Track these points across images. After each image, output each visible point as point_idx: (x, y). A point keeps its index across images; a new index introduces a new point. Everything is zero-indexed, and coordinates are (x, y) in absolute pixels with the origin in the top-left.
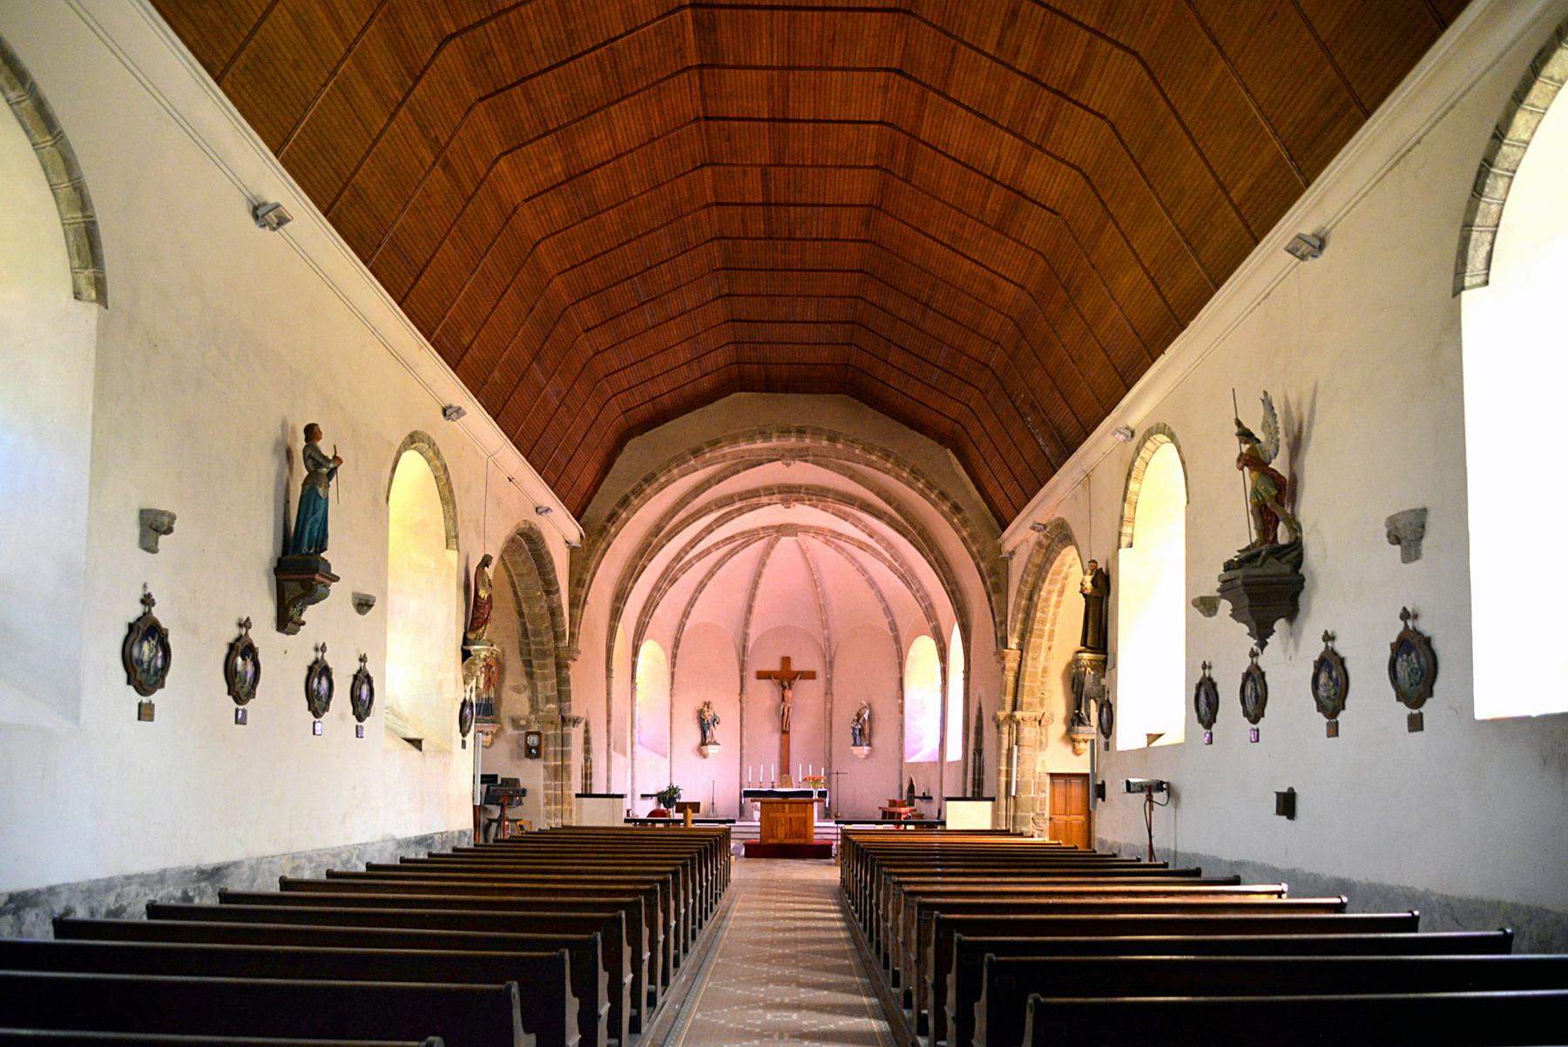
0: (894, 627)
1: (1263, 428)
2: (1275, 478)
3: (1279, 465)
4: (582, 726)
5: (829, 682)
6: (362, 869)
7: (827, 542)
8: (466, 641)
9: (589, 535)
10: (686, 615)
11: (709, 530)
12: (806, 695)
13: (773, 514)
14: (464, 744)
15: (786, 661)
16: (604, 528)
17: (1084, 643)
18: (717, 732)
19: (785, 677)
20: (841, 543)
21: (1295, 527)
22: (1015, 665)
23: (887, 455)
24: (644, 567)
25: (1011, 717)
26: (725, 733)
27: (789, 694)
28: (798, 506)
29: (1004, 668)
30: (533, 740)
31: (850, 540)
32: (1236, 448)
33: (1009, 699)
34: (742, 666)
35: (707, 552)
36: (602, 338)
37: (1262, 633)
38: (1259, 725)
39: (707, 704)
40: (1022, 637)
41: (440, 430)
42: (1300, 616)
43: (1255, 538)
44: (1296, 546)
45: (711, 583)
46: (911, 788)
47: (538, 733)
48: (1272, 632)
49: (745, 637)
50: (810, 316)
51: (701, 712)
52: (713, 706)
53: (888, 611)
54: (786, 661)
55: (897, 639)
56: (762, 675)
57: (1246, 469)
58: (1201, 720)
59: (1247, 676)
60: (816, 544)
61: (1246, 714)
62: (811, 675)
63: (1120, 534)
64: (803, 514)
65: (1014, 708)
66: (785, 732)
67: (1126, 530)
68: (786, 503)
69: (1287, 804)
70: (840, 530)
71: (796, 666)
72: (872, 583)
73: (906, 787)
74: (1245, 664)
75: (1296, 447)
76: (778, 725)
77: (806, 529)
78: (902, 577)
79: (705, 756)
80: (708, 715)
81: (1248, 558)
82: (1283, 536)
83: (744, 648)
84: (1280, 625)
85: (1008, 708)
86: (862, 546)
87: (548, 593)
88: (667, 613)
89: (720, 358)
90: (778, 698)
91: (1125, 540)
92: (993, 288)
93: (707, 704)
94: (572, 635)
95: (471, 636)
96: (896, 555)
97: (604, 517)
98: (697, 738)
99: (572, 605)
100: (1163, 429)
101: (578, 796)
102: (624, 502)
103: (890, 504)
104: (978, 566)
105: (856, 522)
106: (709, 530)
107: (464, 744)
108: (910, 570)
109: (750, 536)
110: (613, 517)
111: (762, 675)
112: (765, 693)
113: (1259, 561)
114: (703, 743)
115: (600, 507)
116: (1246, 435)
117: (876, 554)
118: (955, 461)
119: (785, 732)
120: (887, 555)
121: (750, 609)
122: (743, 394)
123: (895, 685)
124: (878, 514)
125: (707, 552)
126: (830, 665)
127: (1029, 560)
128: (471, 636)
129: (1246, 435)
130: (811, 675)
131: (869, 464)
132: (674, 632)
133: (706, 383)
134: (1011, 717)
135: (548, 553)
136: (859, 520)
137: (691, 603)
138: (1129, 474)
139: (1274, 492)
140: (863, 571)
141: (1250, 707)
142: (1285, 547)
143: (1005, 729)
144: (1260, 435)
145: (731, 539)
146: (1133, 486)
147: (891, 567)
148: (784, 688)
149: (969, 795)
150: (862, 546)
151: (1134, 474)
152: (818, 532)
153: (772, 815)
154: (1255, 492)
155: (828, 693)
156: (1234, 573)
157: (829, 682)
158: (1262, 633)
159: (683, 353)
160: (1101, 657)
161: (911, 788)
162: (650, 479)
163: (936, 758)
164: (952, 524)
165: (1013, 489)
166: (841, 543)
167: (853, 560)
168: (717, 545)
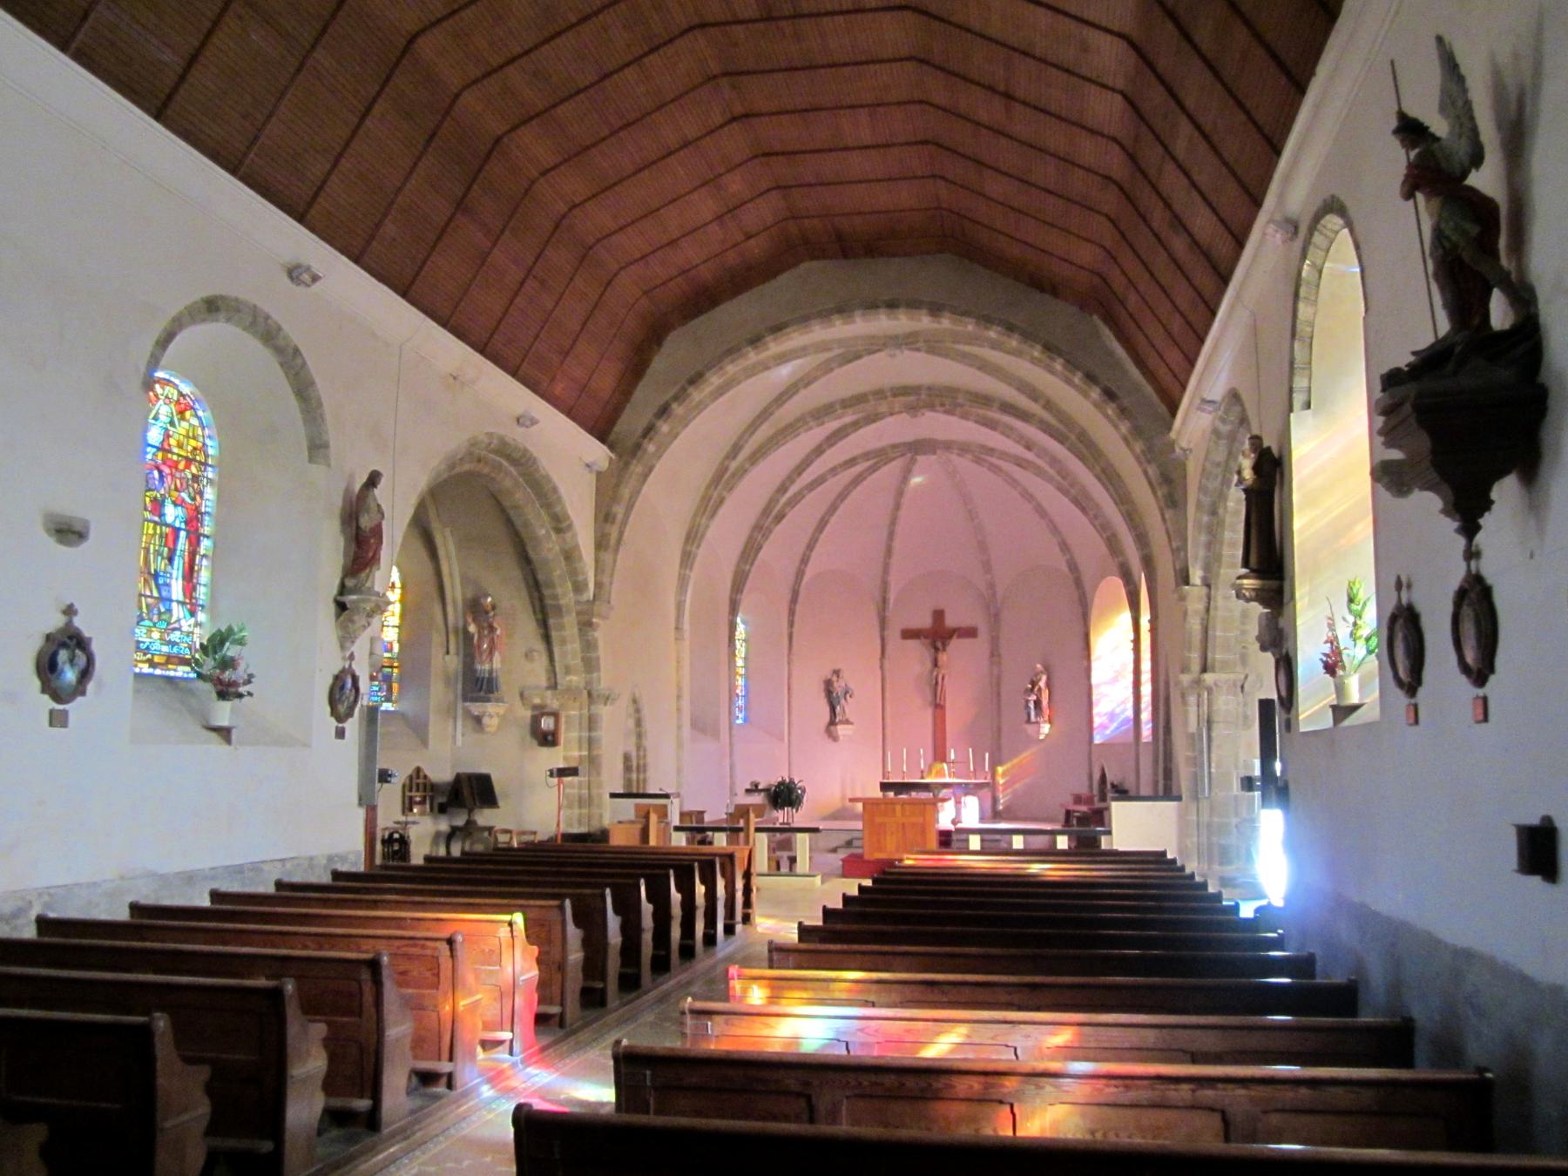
0: (1073, 567)
1: (1443, 109)
2: (1481, 208)
3: (1486, 180)
4: (624, 703)
5: (995, 642)
6: (270, 889)
7: (978, 461)
8: (343, 589)
9: (620, 456)
10: (805, 561)
11: (819, 451)
12: (962, 658)
13: (896, 428)
14: (340, 734)
15: (939, 615)
16: (638, 446)
17: (1246, 563)
18: (848, 708)
19: (938, 635)
20: (994, 460)
21: (1523, 298)
22: (1201, 606)
23: (1010, 328)
24: (721, 501)
25: (1198, 682)
26: (861, 706)
27: (943, 657)
28: (929, 414)
29: (1185, 613)
30: (546, 723)
31: (1004, 456)
32: (1396, 158)
33: (1195, 658)
34: (883, 623)
35: (819, 481)
36: (572, 184)
37: (1469, 510)
38: (1487, 690)
39: (837, 672)
40: (1207, 568)
41: (281, 301)
42: (1545, 469)
43: (1444, 326)
44: (1528, 333)
45: (833, 520)
46: (1103, 776)
47: (556, 715)
48: (1487, 504)
49: (885, 585)
50: (866, 136)
51: (828, 684)
52: (845, 674)
53: (1064, 547)
54: (939, 615)
55: (1078, 583)
56: (908, 634)
57: (1420, 196)
58: (1400, 683)
59: (1461, 596)
60: (964, 463)
61: (1465, 668)
62: (971, 633)
63: (1291, 391)
64: (935, 424)
65: (1204, 669)
66: (938, 707)
67: (1300, 382)
68: (913, 409)
69: (1539, 850)
70: (991, 444)
71: (951, 621)
72: (1041, 512)
73: (1097, 776)
74: (1456, 575)
75: (1516, 138)
76: (930, 698)
77: (948, 446)
78: (1076, 502)
79: (835, 738)
80: (838, 686)
81: (1431, 361)
82: (1500, 313)
83: (884, 601)
84: (1506, 491)
85: (1196, 666)
86: (1020, 463)
87: (559, 531)
88: (778, 553)
89: (765, 211)
90: (929, 665)
91: (1298, 399)
92: (1085, 49)
93: (837, 672)
94: (598, 585)
95: (350, 583)
96: (1064, 472)
97: (640, 431)
98: (827, 718)
99: (601, 544)
100: (1334, 206)
101: (613, 795)
102: (664, 411)
103: (1035, 400)
104: (1145, 473)
105: (1008, 431)
106: (819, 451)
107: (340, 734)
108: (1088, 497)
109: (880, 457)
110: (649, 431)
111: (908, 634)
112: (917, 652)
113: (1450, 367)
114: (832, 723)
115: (631, 421)
116: (1411, 130)
117: (1039, 472)
118: (1107, 334)
119: (938, 707)
120: (1052, 472)
121: (889, 551)
122: (814, 264)
123: (1080, 644)
124: (1024, 416)
125: (819, 481)
126: (995, 618)
127: (1206, 459)
128: (350, 583)
129: (1411, 130)
130: (971, 633)
131: (995, 346)
132: (791, 578)
133: (757, 248)
134: (1198, 682)
135: (548, 479)
136: (1012, 428)
137: (810, 547)
138: (1296, 296)
139: (1474, 230)
140: (1028, 496)
141: (1470, 657)
142: (1503, 335)
143: (1192, 699)
144: (1439, 126)
145: (852, 462)
146: (1304, 310)
147: (1060, 489)
148: (937, 649)
149: (1161, 793)
150: (1020, 463)
151: (1303, 292)
152: (964, 449)
153: (878, 820)
154: (1438, 234)
155: (995, 654)
156: (1400, 391)
157: (995, 642)
158: (1469, 510)
159: (704, 206)
160: (1273, 584)
161: (1103, 776)
162: (695, 379)
163: (1131, 738)
164: (1106, 416)
165: (1174, 356)
166: (994, 460)
167: (1014, 482)
168: (833, 471)
